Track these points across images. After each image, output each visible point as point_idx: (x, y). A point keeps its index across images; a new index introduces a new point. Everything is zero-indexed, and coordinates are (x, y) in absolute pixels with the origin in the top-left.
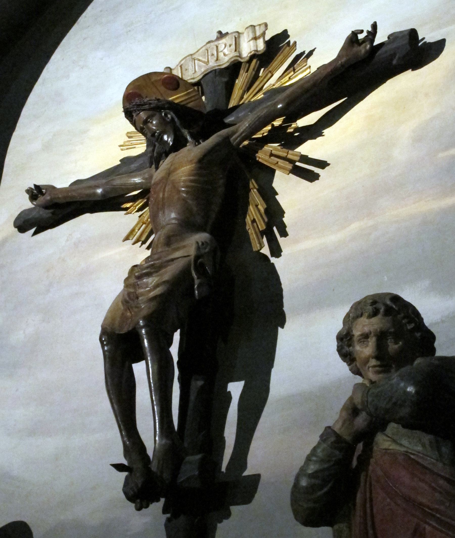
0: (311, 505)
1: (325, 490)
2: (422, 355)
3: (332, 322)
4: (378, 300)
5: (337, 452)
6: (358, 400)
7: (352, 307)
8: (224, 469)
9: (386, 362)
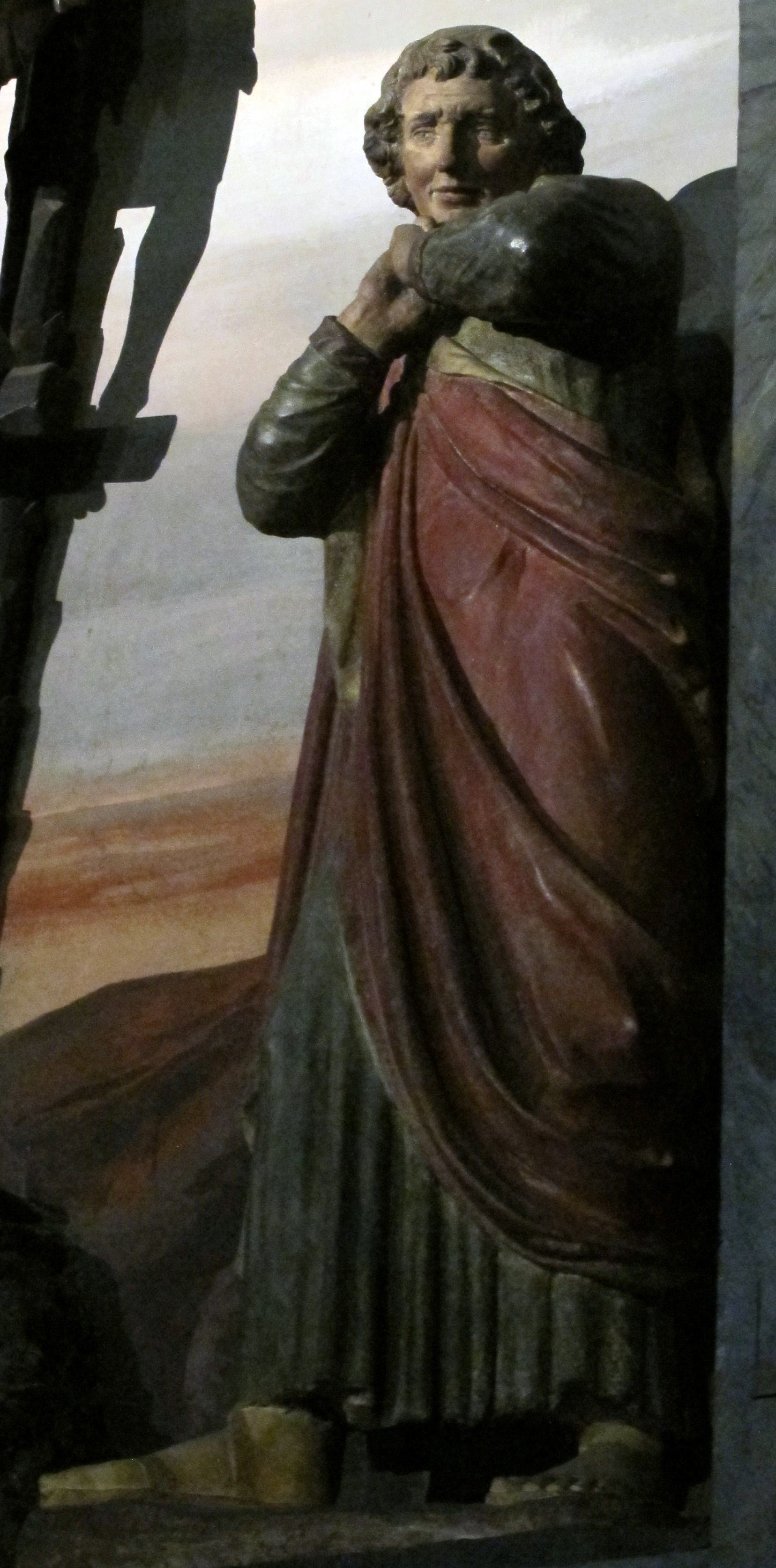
0: (282, 487)
1: (318, 453)
2: (553, 171)
3: (362, 89)
4: (465, 42)
5: (346, 375)
6: (400, 262)
7: (404, 53)
8: (95, 400)
9: (470, 180)
